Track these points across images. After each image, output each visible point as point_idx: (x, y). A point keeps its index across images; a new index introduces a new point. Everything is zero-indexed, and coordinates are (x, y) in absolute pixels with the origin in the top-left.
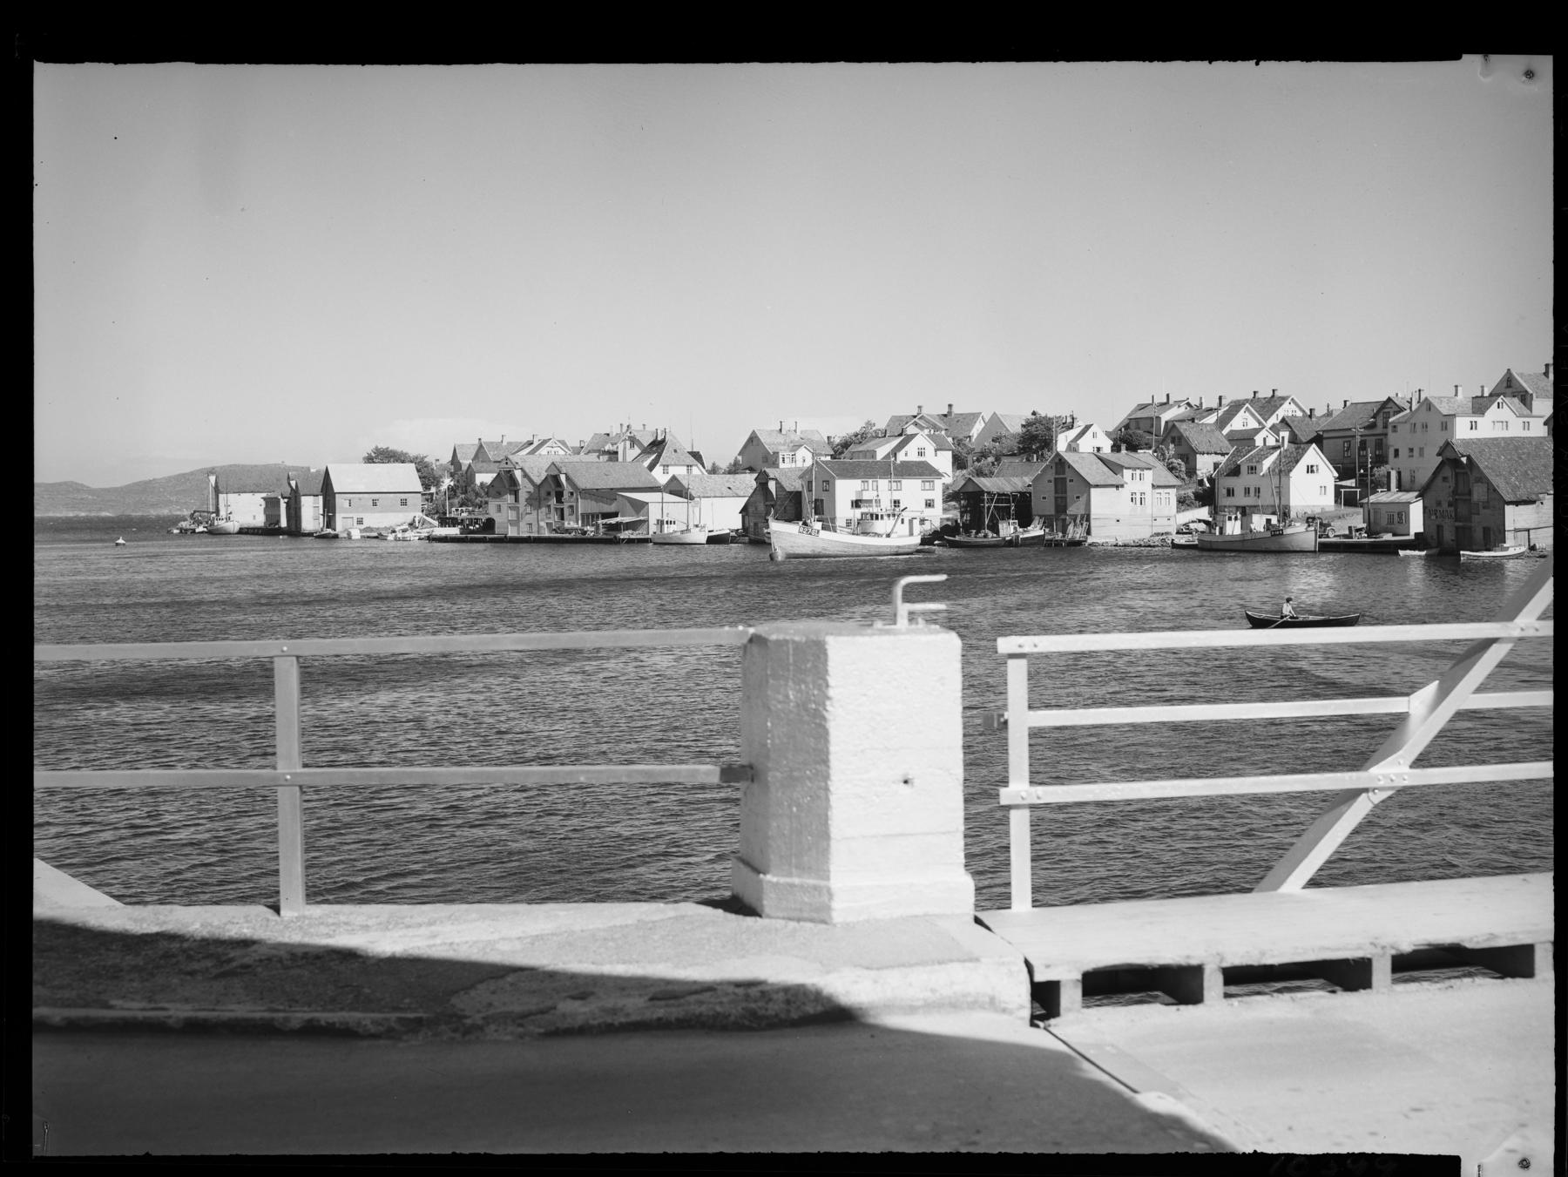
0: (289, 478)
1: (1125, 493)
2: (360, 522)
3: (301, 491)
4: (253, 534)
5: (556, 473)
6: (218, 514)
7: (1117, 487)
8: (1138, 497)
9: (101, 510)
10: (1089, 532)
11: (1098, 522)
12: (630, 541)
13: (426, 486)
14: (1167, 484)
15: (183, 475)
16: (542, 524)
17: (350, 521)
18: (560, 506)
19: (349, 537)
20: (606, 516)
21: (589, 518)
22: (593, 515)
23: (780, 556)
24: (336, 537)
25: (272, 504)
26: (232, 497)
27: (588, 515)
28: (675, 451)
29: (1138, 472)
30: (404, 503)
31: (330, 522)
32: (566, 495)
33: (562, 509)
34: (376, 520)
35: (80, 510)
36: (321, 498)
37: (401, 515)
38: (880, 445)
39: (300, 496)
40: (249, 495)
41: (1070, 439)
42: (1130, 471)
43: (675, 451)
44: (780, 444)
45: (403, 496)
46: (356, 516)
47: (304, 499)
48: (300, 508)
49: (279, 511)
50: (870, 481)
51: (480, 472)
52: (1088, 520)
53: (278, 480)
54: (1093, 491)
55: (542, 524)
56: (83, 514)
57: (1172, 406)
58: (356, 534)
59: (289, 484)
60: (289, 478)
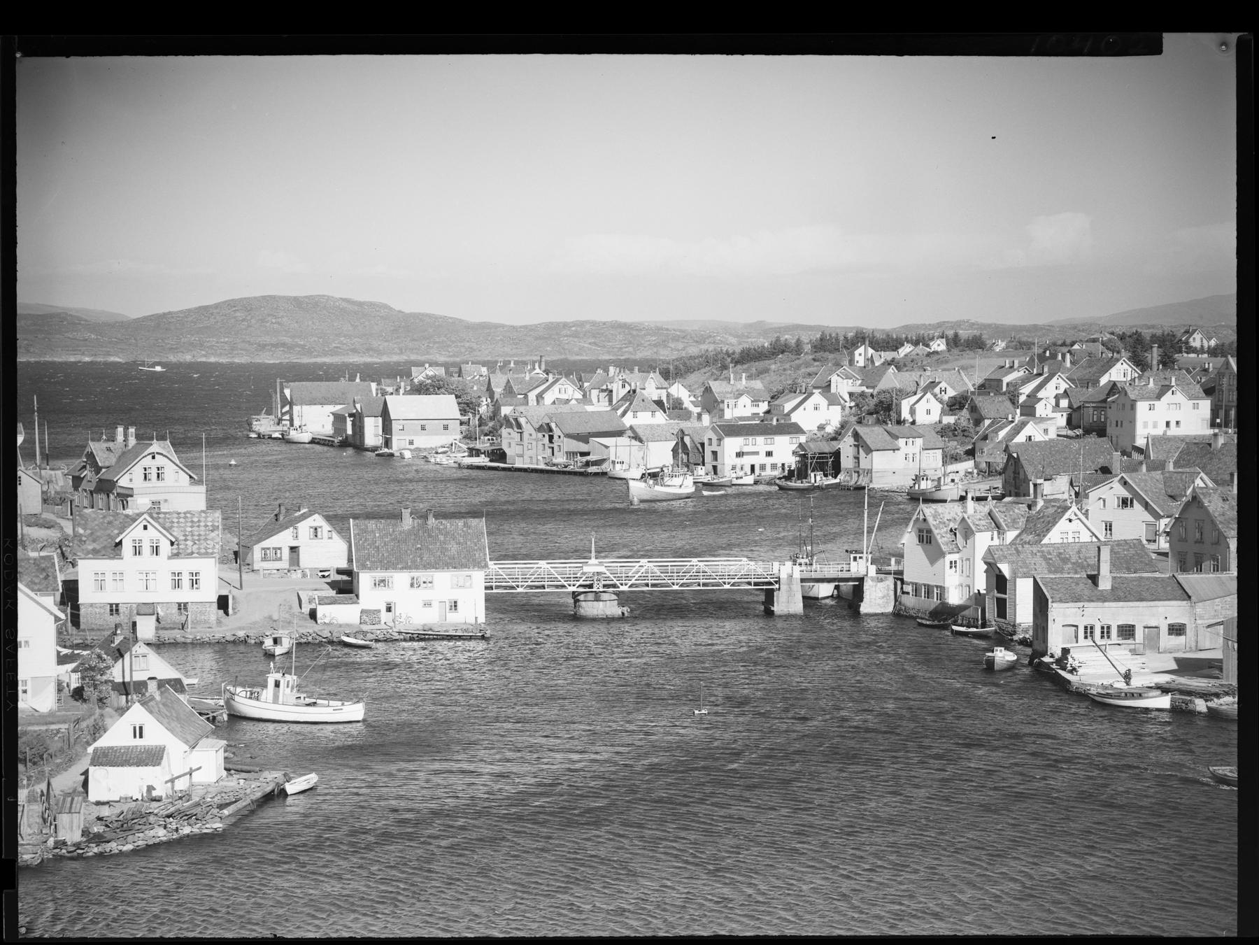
0: (354, 401)
1: (900, 455)
2: (411, 443)
3: (365, 413)
4: (324, 445)
5: (549, 421)
6: (292, 425)
7: (894, 450)
8: (911, 456)
9: (108, 354)
10: (871, 481)
11: (878, 475)
12: (596, 474)
13: (463, 412)
14: (934, 447)
15: (206, 308)
16: (540, 458)
17: (403, 441)
18: (552, 445)
19: (402, 457)
20: (583, 454)
21: (571, 454)
22: (573, 453)
23: (636, 500)
24: (392, 455)
25: (339, 419)
26: (307, 409)
27: (570, 453)
28: (643, 400)
29: (911, 440)
30: (446, 428)
31: (387, 443)
32: (556, 438)
33: (553, 448)
34: (423, 442)
35: (83, 354)
36: (380, 419)
37: (444, 437)
38: (788, 401)
39: (363, 417)
40: (319, 407)
41: (911, 404)
42: (905, 440)
43: (643, 400)
44: (727, 393)
45: (446, 422)
46: (408, 438)
47: (366, 419)
48: (363, 427)
49: (346, 426)
50: (750, 438)
51: (505, 405)
52: (871, 473)
53: (343, 394)
54: (874, 453)
55: (540, 458)
56: (87, 359)
57: (1015, 370)
58: (408, 455)
59: (355, 406)
60: (354, 401)
